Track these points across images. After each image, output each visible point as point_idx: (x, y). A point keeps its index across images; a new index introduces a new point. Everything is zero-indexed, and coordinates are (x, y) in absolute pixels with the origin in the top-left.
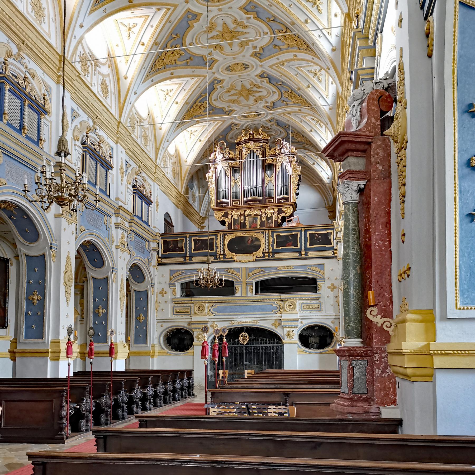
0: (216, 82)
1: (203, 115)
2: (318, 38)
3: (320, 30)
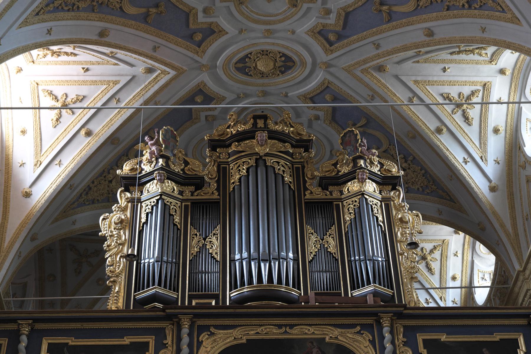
0: (198, 37)
1: (147, 220)
2: (463, 164)
3: (427, 290)
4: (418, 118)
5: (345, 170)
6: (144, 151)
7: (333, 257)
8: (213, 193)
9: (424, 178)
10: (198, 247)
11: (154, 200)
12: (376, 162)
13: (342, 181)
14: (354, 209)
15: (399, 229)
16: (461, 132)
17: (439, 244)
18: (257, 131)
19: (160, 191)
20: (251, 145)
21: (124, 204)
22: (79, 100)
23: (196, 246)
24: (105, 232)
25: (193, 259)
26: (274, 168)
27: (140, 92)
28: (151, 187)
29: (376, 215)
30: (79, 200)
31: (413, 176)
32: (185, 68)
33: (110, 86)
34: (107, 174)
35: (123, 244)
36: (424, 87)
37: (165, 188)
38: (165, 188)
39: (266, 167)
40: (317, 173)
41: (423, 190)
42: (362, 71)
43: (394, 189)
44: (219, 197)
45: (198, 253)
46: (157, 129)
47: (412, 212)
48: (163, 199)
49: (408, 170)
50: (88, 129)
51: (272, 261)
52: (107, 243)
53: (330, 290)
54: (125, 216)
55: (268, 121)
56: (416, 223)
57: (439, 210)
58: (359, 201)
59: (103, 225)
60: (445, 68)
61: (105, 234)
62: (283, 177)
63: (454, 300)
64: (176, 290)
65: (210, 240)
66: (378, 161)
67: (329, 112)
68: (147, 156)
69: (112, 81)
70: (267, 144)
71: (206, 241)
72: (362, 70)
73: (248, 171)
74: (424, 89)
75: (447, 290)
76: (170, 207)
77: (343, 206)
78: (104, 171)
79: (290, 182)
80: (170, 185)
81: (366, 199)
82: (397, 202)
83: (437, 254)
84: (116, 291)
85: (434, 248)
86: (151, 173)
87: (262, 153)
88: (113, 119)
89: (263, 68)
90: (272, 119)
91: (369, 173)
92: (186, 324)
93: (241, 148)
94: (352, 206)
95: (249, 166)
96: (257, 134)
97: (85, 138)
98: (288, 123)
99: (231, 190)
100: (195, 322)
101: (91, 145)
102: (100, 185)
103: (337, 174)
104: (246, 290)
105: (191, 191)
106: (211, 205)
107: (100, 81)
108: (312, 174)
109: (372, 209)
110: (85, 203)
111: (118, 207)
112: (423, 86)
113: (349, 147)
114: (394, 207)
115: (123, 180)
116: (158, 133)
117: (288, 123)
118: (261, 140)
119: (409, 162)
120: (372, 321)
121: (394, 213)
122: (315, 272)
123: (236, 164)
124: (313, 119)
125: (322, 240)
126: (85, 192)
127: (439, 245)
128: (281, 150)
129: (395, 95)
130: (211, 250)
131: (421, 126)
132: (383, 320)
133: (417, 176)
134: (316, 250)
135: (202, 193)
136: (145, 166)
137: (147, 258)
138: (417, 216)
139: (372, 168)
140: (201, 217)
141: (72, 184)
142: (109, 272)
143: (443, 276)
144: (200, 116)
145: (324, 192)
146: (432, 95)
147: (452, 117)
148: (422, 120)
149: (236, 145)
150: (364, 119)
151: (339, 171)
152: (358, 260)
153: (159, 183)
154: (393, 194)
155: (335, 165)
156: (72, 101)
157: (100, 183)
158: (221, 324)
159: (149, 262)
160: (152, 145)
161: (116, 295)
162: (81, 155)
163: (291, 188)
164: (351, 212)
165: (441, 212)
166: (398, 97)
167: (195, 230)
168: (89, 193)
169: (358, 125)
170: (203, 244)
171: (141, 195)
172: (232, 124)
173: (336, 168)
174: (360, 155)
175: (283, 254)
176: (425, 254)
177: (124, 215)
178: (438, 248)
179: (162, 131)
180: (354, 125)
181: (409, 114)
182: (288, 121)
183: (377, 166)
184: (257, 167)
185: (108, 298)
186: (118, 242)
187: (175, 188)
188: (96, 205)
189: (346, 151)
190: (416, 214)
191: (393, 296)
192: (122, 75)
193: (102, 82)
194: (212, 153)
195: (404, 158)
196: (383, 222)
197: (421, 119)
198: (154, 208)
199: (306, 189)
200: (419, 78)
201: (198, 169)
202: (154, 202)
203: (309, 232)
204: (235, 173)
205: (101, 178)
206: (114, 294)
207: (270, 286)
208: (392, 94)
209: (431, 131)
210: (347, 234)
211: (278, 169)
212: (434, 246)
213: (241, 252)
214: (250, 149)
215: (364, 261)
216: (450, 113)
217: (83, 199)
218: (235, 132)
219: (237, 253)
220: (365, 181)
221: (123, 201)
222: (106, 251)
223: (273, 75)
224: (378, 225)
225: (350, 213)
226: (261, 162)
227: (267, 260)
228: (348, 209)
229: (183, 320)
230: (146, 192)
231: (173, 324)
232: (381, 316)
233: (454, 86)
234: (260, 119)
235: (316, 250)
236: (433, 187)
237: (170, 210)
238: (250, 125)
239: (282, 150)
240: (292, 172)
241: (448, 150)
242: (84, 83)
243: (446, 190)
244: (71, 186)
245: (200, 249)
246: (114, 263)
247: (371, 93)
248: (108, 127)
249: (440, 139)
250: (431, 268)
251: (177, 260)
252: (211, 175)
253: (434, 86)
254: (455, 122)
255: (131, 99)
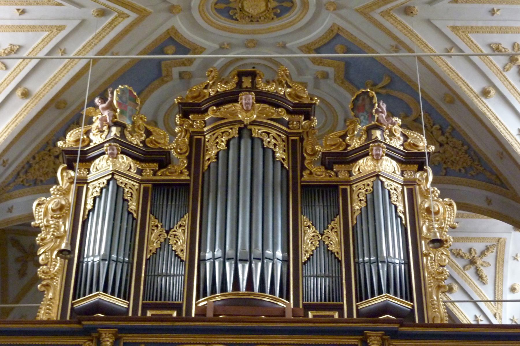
3: (475, 302)
4: (457, 76)
5: (356, 144)
6: (94, 117)
7: (336, 258)
8: (182, 173)
9: (467, 155)
10: (159, 242)
11: (104, 180)
12: (398, 133)
13: (352, 158)
14: (366, 194)
15: (424, 222)
16: (515, 95)
17: (492, 243)
18: (241, 92)
19: (111, 169)
20: (234, 110)
21: (65, 185)
22: (13, 51)
23: (156, 241)
24: (40, 221)
25: (151, 257)
26: (262, 140)
27: (92, 41)
28: (101, 163)
29: (395, 203)
30: (16, 180)
31: (453, 153)
32: (149, 9)
33: (53, 32)
34: (52, 147)
35: (61, 237)
36: (465, 34)
37: (118, 165)
38: (118, 165)
39: (253, 139)
40: (319, 147)
41: (466, 172)
42: (383, 14)
43: (421, 168)
44: (188, 178)
45: (158, 250)
46: (111, 89)
47: (443, 199)
48: (116, 180)
49: (446, 146)
50: (25, 88)
51: (254, 262)
52: (41, 235)
53: (329, 301)
54: (67, 201)
55: (257, 79)
56: (448, 214)
57: (487, 198)
58: (373, 185)
59: (37, 212)
60: (493, 10)
61: (39, 224)
62: (274, 153)
63: (513, 317)
64: (126, 297)
65: (174, 233)
66: (401, 132)
67: (341, 69)
68: (97, 123)
69: (56, 26)
70: (254, 110)
71: (169, 234)
72: (381, 12)
73: (228, 144)
74: (466, 37)
75: (504, 303)
76: (124, 190)
77: (352, 191)
78: (48, 143)
79: (283, 159)
80: (124, 161)
81: (382, 182)
82: (424, 187)
83: (490, 257)
84: (49, 297)
85: (486, 249)
86: (101, 145)
87: (247, 121)
88: (58, 76)
89: (251, 9)
90: (262, 76)
91: (387, 148)
92: (108, 341)
93: (221, 114)
94: (363, 191)
95: (230, 137)
96: (241, 96)
97: (21, 100)
98: (284, 82)
99: (206, 168)
100: (120, 338)
101: (29, 109)
102: (43, 161)
103: (346, 149)
104: (219, 297)
105: (153, 170)
106: (175, 189)
107: (40, 26)
108: (313, 149)
109: (390, 195)
110: (23, 185)
111: (58, 190)
112: (463, 34)
113: (362, 114)
114: (420, 194)
115: (65, 154)
116: (112, 93)
117: (284, 82)
118: (246, 104)
119: (447, 134)
120: (357, 340)
121: (419, 200)
122: (310, 276)
123: (213, 134)
124: (319, 76)
125: (322, 235)
126: (24, 171)
127: (493, 245)
128: (272, 117)
129: (427, 45)
130: (175, 246)
131: (461, 87)
132: (371, 340)
133: (458, 153)
134: (313, 248)
135: (167, 173)
136: (94, 137)
137: (91, 256)
138: (450, 205)
139: (392, 142)
140: (165, 203)
141: (5, 160)
142: (41, 273)
143: (498, 286)
144: (171, 72)
145: (328, 173)
146: (477, 46)
147: (504, 76)
148: (462, 79)
149: (214, 110)
150: (387, 78)
151: (348, 145)
152: (367, 262)
153: (110, 159)
154: (420, 176)
155: (343, 137)
156: (4, 52)
157: (43, 159)
158: (155, 341)
159: (93, 262)
160: (104, 109)
161: (48, 302)
162: (17, 122)
163: (284, 167)
164: (361, 198)
165: (490, 201)
166: (430, 48)
167: (157, 220)
168: (29, 171)
169: (380, 85)
170: (165, 239)
171: (88, 174)
172: (211, 83)
173: (344, 140)
174: (376, 125)
175: (269, 252)
176: (474, 257)
177: (65, 200)
178: (491, 250)
179: (117, 91)
180: (374, 86)
181: (445, 71)
182: (284, 80)
183: (399, 139)
184: (240, 138)
185: (38, 307)
186: (55, 234)
187: (132, 165)
188: (39, 187)
189: (358, 118)
190: (449, 203)
191: (413, 310)
192: (68, 19)
193: (42, 28)
194: (184, 121)
195: (440, 129)
196: (404, 213)
197: (461, 78)
198: (104, 190)
199: (304, 168)
200: (458, 24)
201: (162, 141)
202: (104, 183)
203: (305, 225)
204: (211, 147)
205: (45, 152)
206: (47, 302)
207: (249, 295)
208: (423, 44)
209: (475, 93)
210: (355, 227)
211: (267, 142)
212: (487, 246)
213: (213, 249)
214: (232, 115)
215: (376, 264)
216: (501, 69)
217: (21, 179)
218: (213, 93)
219: (208, 250)
220: (381, 158)
221: (65, 181)
222: (39, 246)
223: (265, 19)
224: (397, 216)
225: (360, 200)
226: (245, 133)
227: (246, 261)
228: (358, 195)
229: (104, 335)
230: (95, 170)
231: (92, 341)
232: (368, 334)
233: (506, 35)
234: (247, 76)
235: (313, 248)
236: (479, 167)
237: (124, 193)
238: (233, 84)
239: (274, 116)
240: (286, 146)
241: (497, 118)
242: (20, 28)
243: (495, 171)
244: (4, 162)
245: (161, 245)
246: (48, 262)
247: (394, 43)
248: (51, 86)
249: (487, 103)
250: (481, 275)
251: (131, 259)
252: (181, 150)
253: (479, 34)
254: (508, 82)
255: (80, 50)
